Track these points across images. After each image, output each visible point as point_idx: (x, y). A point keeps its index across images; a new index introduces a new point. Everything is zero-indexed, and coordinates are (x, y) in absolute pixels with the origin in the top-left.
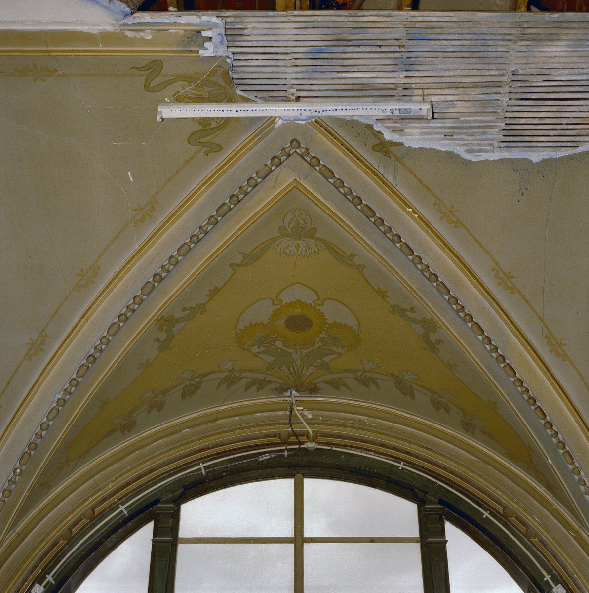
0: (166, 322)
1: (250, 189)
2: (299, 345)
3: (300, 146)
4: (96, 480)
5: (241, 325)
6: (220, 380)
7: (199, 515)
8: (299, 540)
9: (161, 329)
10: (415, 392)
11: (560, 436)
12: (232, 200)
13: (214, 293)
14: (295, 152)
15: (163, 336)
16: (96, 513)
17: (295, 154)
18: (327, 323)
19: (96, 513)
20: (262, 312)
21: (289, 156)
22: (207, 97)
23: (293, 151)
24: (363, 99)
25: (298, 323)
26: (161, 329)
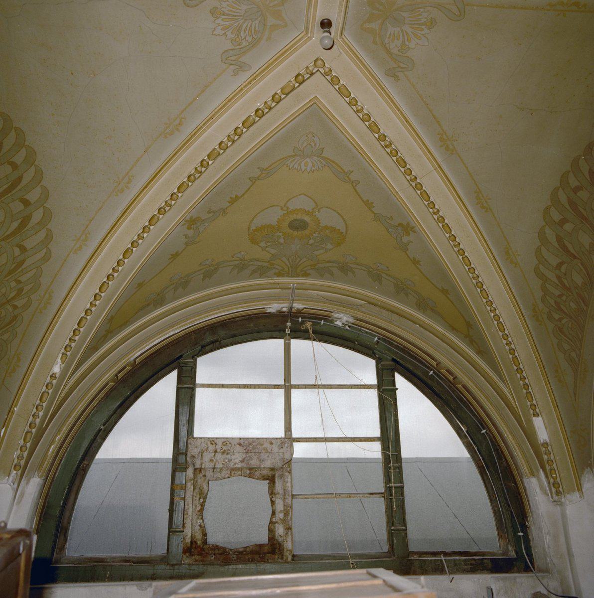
0: (192, 222)
1: (274, 104)
2: (298, 242)
3: (324, 65)
4: (293, 310)
5: (253, 227)
6: (232, 267)
7: (208, 368)
8: (288, 387)
9: (189, 228)
10: (383, 279)
11: (497, 311)
12: (258, 114)
13: (233, 201)
14: (318, 70)
15: (190, 233)
16: (119, 378)
17: (318, 72)
18: (320, 226)
19: (119, 378)
20: (272, 217)
21: (312, 74)
22: (242, 14)
23: (316, 69)
24: (43, 486)
25: (298, 225)
26: (189, 228)
